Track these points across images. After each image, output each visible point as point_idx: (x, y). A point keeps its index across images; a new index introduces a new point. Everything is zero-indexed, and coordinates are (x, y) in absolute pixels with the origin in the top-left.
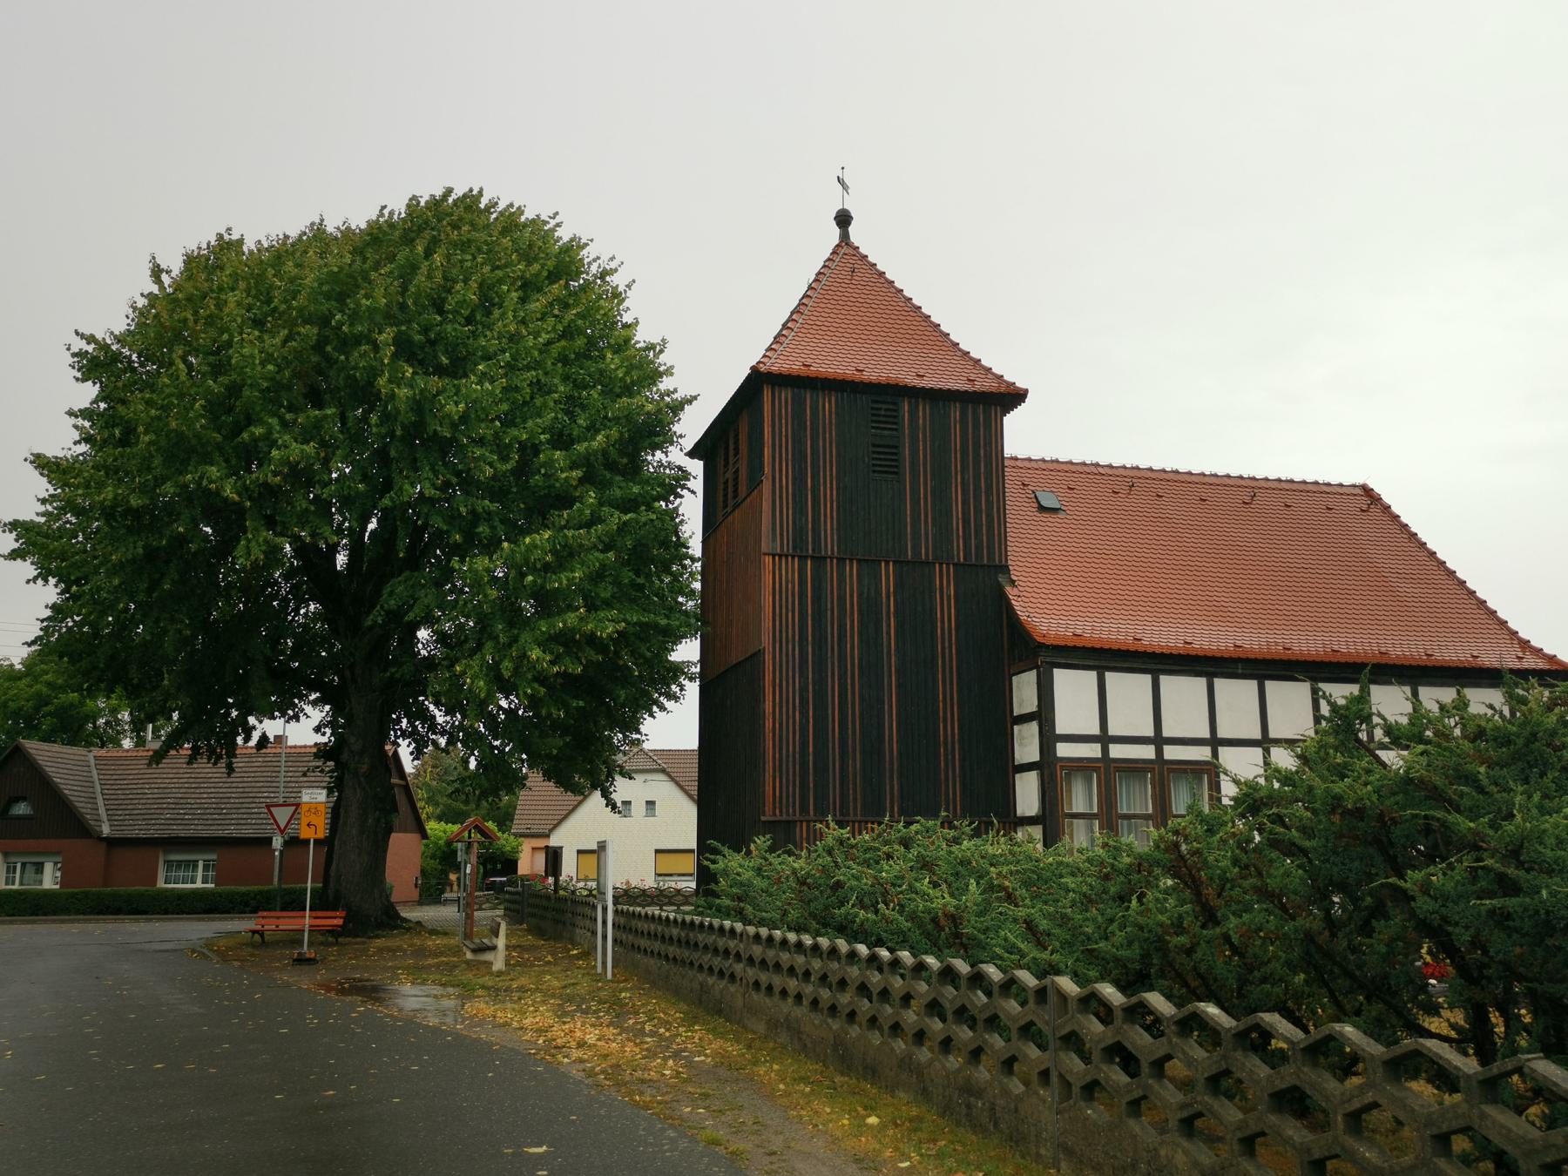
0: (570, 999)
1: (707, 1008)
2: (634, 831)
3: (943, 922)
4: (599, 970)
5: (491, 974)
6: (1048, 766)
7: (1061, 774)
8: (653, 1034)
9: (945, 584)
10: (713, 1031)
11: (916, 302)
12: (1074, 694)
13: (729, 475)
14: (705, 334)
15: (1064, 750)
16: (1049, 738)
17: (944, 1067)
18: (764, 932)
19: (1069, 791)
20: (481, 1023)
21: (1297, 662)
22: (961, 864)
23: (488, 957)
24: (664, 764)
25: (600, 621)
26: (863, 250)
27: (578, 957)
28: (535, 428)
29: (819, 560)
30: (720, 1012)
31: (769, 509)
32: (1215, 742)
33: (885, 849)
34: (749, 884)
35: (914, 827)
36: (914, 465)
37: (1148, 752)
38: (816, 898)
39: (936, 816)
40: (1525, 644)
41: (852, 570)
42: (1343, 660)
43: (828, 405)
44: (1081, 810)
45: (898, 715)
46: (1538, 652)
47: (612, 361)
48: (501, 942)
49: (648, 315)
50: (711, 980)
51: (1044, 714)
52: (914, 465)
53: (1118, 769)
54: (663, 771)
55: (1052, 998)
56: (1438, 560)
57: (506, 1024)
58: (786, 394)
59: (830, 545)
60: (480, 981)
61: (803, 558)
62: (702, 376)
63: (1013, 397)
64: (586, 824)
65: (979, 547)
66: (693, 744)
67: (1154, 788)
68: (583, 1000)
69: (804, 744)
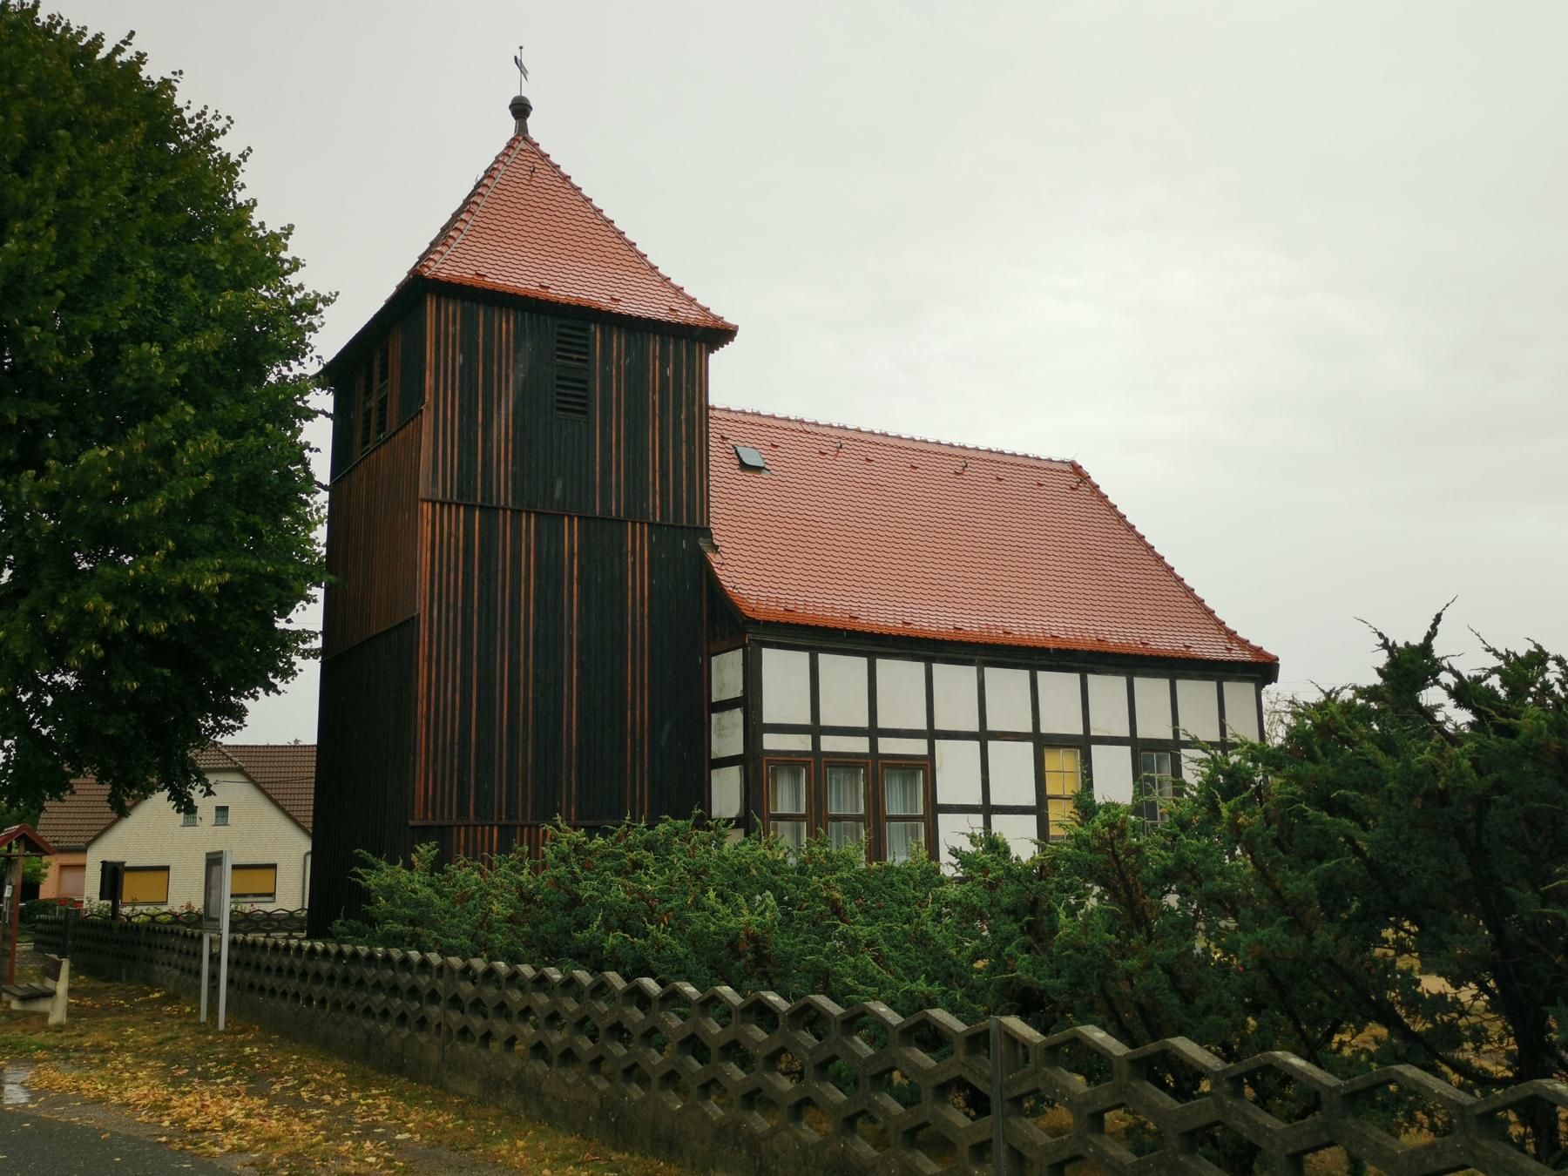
0: (175, 1059)
1: (376, 1062)
2: (216, 843)
3: (743, 947)
4: (203, 1017)
5: (48, 1029)
6: (753, 762)
7: (767, 769)
8: (319, 1104)
9: (638, 545)
10: (399, 1095)
11: (607, 214)
12: (783, 673)
13: (373, 404)
14: (348, 237)
15: (771, 742)
16: (754, 728)
17: (798, 1139)
18: (396, 953)
19: (775, 789)
20: (62, 1099)
21: (1019, 647)
22: (738, 872)
23: (42, 1006)
24: (261, 768)
25: (199, 571)
26: (544, 148)
27: (163, 1001)
28: (115, 314)
29: (489, 511)
30: (400, 1070)
31: (431, 445)
32: (932, 734)
33: (631, 855)
34: (429, 903)
35: (661, 827)
36: (606, 402)
37: (860, 745)
38: (547, 919)
39: (686, 817)
40: (1231, 635)
41: (529, 524)
42: (1063, 647)
43: (506, 325)
44: (787, 811)
45: (579, 701)
46: (1244, 644)
47: (215, 251)
48: (62, 986)
49: (269, 194)
50: (385, 1028)
51: (750, 701)
52: (606, 402)
53: (830, 765)
54: (240, 771)
55: (999, 1046)
56: (1146, 544)
57: (99, 1100)
58: (453, 308)
59: (503, 493)
60: (35, 1038)
61: (470, 508)
62: (346, 273)
63: (721, 334)
64: (151, 833)
65: (678, 511)
66: (310, 737)
67: (866, 786)
68: (194, 1062)
69: (465, 734)
